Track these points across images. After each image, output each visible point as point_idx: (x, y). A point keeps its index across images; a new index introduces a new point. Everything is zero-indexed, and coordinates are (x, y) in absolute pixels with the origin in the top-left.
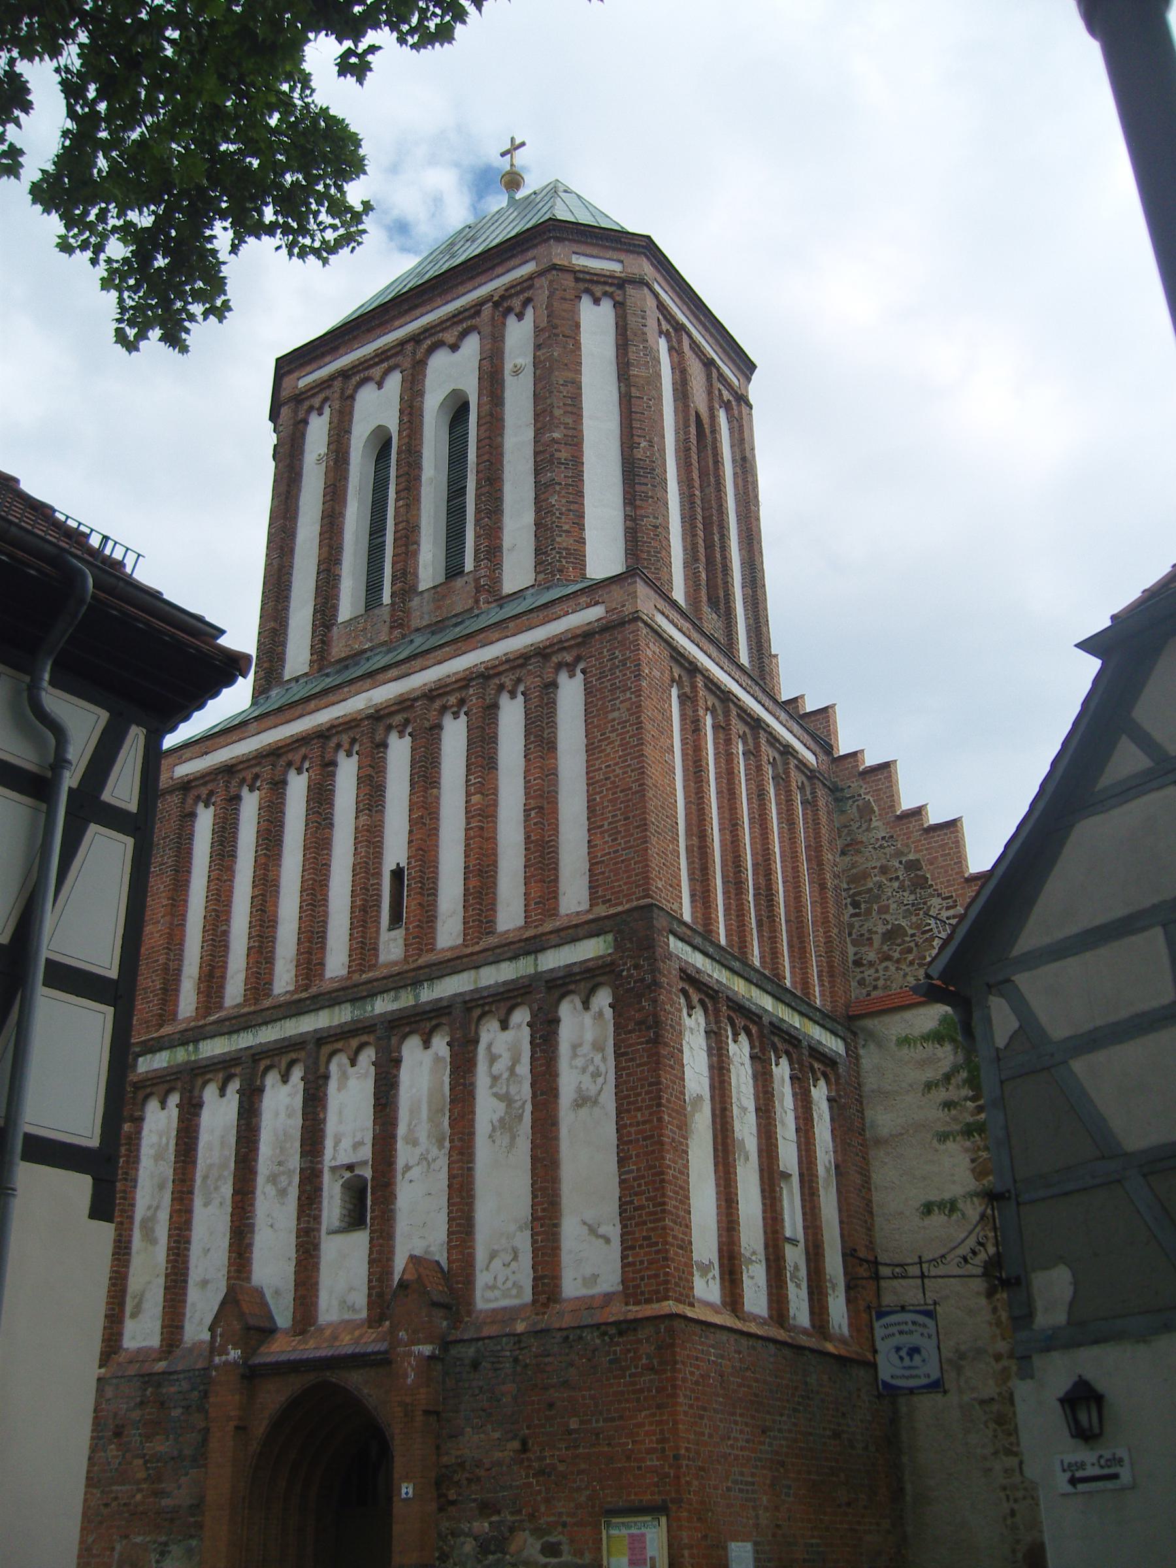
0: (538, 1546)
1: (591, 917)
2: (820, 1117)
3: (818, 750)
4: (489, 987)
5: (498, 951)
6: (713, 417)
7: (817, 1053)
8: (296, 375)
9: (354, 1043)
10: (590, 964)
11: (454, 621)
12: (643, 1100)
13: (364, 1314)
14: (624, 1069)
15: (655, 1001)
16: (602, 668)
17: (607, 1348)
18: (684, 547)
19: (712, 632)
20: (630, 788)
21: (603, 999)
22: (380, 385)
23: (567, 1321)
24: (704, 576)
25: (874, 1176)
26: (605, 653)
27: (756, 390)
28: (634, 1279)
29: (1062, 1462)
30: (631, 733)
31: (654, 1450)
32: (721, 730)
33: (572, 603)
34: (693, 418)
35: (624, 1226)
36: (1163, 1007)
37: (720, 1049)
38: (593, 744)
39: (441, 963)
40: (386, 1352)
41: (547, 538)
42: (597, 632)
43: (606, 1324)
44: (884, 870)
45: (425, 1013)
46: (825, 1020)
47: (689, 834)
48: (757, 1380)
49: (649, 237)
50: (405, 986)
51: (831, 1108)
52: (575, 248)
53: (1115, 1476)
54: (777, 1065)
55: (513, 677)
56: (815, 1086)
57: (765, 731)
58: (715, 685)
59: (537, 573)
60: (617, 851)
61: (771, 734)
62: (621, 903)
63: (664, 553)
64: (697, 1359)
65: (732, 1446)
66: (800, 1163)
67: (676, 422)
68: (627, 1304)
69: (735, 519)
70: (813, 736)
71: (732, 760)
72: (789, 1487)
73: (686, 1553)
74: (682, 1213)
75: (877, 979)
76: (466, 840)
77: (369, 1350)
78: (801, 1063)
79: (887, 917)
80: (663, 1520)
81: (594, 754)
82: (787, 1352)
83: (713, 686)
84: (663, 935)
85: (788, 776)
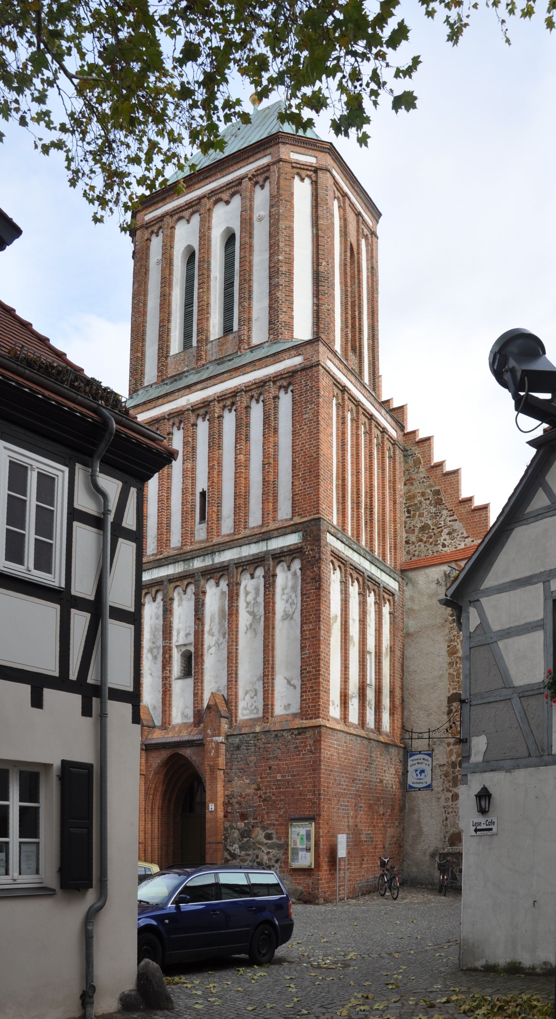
0: (263, 835)
1: (292, 523)
4: (245, 557)
5: (250, 538)
6: (359, 245)
7: (386, 590)
8: (144, 213)
9: (185, 582)
10: (292, 547)
11: (229, 358)
13: (192, 720)
14: (305, 602)
15: (320, 568)
21: (297, 565)
22: (188, 221)
23: (278, 727)
27: (381, 228)
28: (306, 707)
33: (287, 354)
34: (349, 247)
35: (302, 681)
37: (346, 590)
39: (224, 543)
40: (202, 740)
43: (294, 729)
44: (423, 494)
45: (217, 568)
47: (338, 478)
49: (331, 144)
50: (207, 554)
51: (390, 618)
52: (292, 148)
59: (270, 334)
62: (306, 516)
63: (332, 324)
64: (330, 746)
67: (341, 249)
73: (321, 839)
74: (326, 675)
75: (415, 551)
76: (235, 478)
77: (195, 738)
78: (379, 596)
79: (422, 519)
80: (313, 824)
82: (365, 742)
83: (353, 399)
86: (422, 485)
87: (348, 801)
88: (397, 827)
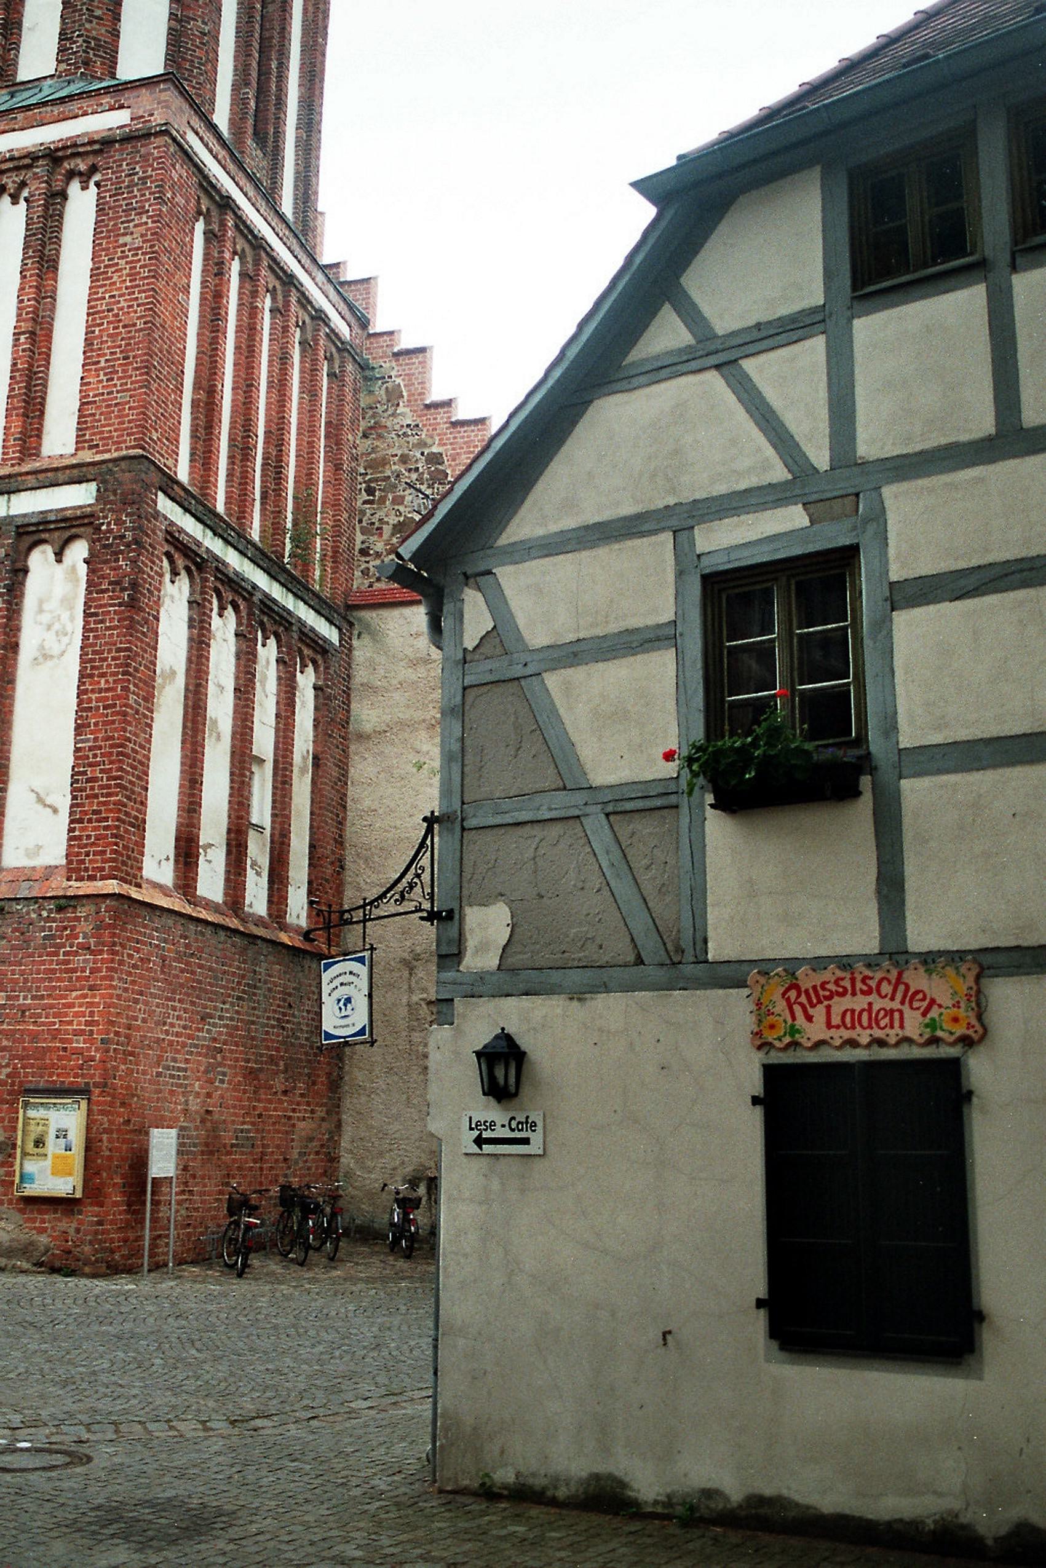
2: (303, 703)
3: (353, 322)
10: (69, 513)
12: (109, 666)
14: (92, 630)
16: (118, 183)
17: (42, 923)
18: (235, 66)
19: (255, 171)
20: (135, 325)
21: (79, 551)
24: (252, 104)
25: (352, 770)
26: (124, 167)
28: (78, 854)
29: (470, 1118)
30: (142, 263)
31: (81, 1033)
32: (248, 279)
35: (74, 798)
36: (659, 626)
38: (99, 268)
41: (74, 22)
42: (117, 141)
44: (404, 459)
46: (321, 606)
47: (197, 386)
48: (201, 966)
51: (316, 697)
53: (526, 1141)
54: (264, 645)
55: (16, 179)
56: (302, 672)
57: (298, 290)
58: (247, 227)
59: (59, 61)
60: (112, 392)
61: (303, 294)
62: (109, 451)
65: (167, 1032)
66: (276, 748)
68: (68, 880)
69: (299, 49)
70: (351, 307)
71: (256, 314)
72: (224, 1074)
78: (290, 648)
79: (401, 508)
80: (84, 1104)
81: (98, 280)
84: (151, 492)
85: (317, 344)
86: (402, 441)
87: (187, 1061)
88: (323, 1119)
